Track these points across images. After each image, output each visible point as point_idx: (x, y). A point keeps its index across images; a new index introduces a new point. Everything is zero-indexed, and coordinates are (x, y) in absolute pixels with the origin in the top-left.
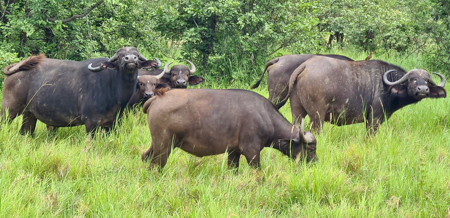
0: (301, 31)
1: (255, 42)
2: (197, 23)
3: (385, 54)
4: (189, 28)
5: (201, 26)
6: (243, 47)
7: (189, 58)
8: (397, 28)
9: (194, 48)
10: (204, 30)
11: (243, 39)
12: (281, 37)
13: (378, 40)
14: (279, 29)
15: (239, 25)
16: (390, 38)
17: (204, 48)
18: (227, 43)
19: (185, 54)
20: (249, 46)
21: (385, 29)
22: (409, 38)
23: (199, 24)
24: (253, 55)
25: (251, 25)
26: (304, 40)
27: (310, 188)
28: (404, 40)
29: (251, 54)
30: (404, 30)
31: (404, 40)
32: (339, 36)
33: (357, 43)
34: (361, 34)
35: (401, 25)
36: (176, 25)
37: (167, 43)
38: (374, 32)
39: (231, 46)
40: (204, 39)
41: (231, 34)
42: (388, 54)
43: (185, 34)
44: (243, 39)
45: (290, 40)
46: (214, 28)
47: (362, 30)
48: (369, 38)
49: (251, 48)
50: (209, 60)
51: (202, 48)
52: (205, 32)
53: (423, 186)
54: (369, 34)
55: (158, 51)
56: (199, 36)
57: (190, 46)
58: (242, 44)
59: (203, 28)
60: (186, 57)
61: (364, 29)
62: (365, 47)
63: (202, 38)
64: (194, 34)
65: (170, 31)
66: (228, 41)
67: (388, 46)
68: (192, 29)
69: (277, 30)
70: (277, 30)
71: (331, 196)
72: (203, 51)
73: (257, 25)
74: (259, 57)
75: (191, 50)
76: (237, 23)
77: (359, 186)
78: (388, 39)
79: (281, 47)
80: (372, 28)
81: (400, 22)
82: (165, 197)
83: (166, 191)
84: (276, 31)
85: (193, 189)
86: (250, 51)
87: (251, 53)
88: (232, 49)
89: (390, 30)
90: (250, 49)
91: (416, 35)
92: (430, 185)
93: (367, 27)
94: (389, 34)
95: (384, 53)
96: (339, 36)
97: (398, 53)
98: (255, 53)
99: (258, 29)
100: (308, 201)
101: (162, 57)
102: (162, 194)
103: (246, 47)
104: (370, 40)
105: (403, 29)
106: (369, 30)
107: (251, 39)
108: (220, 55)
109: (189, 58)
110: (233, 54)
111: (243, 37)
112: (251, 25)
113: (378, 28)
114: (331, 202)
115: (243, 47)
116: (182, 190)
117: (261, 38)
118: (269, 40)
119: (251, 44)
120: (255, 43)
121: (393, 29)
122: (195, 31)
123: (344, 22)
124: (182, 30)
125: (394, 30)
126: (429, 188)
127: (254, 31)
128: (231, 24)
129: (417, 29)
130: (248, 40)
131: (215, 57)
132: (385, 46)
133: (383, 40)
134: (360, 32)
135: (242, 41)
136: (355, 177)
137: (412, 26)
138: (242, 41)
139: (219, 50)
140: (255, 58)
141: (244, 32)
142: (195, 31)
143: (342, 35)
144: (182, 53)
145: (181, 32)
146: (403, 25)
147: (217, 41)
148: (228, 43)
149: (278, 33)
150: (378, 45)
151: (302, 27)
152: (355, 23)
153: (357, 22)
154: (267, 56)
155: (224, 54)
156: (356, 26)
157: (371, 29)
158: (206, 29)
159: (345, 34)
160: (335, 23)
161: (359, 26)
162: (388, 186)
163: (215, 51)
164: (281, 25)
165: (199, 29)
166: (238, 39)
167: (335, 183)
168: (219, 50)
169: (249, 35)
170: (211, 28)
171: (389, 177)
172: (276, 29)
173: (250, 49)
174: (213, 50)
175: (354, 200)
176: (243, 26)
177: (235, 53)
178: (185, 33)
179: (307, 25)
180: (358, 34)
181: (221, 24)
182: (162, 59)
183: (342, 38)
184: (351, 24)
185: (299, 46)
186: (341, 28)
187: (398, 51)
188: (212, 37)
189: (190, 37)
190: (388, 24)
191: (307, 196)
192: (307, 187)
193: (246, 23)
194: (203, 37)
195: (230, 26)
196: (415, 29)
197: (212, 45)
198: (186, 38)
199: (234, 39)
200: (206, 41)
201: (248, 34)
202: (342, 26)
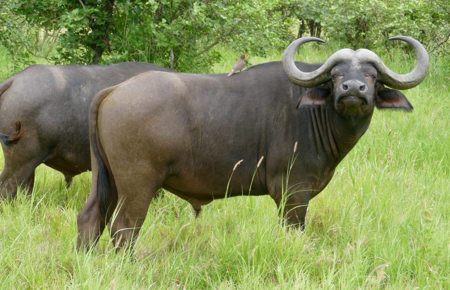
0: (249, 17)
1: (177, 33)
2: (84, 2)
3: (385, 56)
4: (70, 9)
5: (89, 6)
6: (156, 40)
7: (70, 57)
8: (405, 15)
9: (77, 40)
10: (95, 13)
11: (157, 29)
12: (217, 26)
13: (375, 33)
14: (213, 12)
15: (150, 5)
16: (394, 31)
17: (94, 42)
18: (130, 33)
19: (64, 50)
20: (166, 40)
21: (387, 18)
22: (423, 32)
23: (87, 3)
24: (172, 55)
25: (170, 6)
26: (253, 30)
27: (249, 257)
28: (416, 34)
29: (169, 53)
30: (413, 18)
31: (416, 34)
32: (314, 27)
33: (342, 39)
34: (349, 24)
35: (411, 11)
36: (49, 5)
37: (37, 34)
38: (369, 20)
39: (138, 39)
40: (94, 27)
41: (137, 19)
42: (391, 56)
43: (64, 19)
44: (157, 29)
45: (232, 31)
46: (110, 10)
47: (349, 18)
48: (361, 31)
49: (169, 42)
50: (103, 61)
51: (91, 41)
52: (95, 16)
53: (425, 254)
54: (361, 25)
55: (22, 48)
56: (86, 22)
57: (74, 39)
58: (155, 37)
59: (92, 9)
60: (66, 56)
61: (353, 17)
62: (354, 44)
63: (91, 26)
64: (78, 19)
65: (40, 15)
66: (133, 31)
67: (390, 43)
68: (76, 11)
69: (211, 14)
70: (211, 14)
71: (279, 269)
72: (93, 46)
73: (180, 7)
74: (182, 59)
75: (74, 44)
76: (147, 3)
77: (325, 254)
78: (390, 32)
79: (217, 43)
80: (365, 15)
81: (410, 6)
82: (21, 270)
83: (23, 261)
84: (210, 16)
85: (66, 259)
86: (167, 48)
87: (169, 50)
88: (139, 44)
89: (394, 19)
90: (167, 44)
91: (434, 26)
92: (436, 252)
93: (358, 13)
94: (391, 25)
95: (384, 54)
96: (314, 27)
97: (406, 56)
98: (177, 51)
99: (182, 13)
100: (245, 277)
101: (27, 56)
102: (15, 266)
103: (161, 41)
104: (363, 34)
105: (413, 16)
106: (360, 19)
107: (170, 28)
108: (120, 52)
109: (70, 57)
110: (141, 52)
111: (157, 25)
112: (170, 6)
113: (375, 15)
114: (281, 277)
115: (156, 40)
116: (47, 259)
117: (186, 27)
118: (199, 30)
119: (170, 37)
120: (175, 35)
121: (399, 17)
122: (80, 14)
123: (323, 5)
124: (59, 13)
125: (400, 18)
126: (435, 257)
127: (174, 17)
128: (136, 5)
129: (435, 16)
130: (165, 30)
131: (111, 57)
132: (386, 44)
133: (384, 33)
134: (346, 21)
135: (154, 32)
136: (321, 242)
137: (426, 12)
138: (154, 32)
139: (118, 46)
140: (176, 58)
141: (159, 16)
142: (80, 14)
143: (318, 25)
144: (59, 50)
145: (58, 16)
146: (415, 11)
147: (115, 32)
148: (132, 34)
149: (214, 19)
150: (376, 42)
151: (250, 11)
152: (340, 6)
153: (342, 5)
154: (195, 56)
155: (127, 52)
156: (340, 11)
157: (364, 17)
158: (96, 10)
159: (322, 24)
160: (308, 6)
161: (346, 12)
162: (371, 255)
163: (112, 47)
164: (217, 8)
165: (87, 10)
166: (148, 28)
167: (289, 249)
168: (118, 46)
169: (167, 23)
170: (106, 10)
171: (374, 240)
172: (209, 14)
173: (167, 44)
174: (108, 45)
175: (316, 274)
176: (156, 7)
177: (143, 49)
178: (63, 17)
179: (258, 10)
180: (342, 24)
181: (122, 4)
182: (26, 59)
183: (319, 30)
184: (333, 8)
185: (245, 40)
186: (317, 15)
187: (407, 53)
188: (107, 24)
189: (71, 24)
190: (390, 9)
191: (245, 269)
192: (246, 257)
193: (160, 3)
194: (93, 24)
195: (136, 7)
196: (433, 17)
197: (107, 38)
198: (65, 24)
199: (142, 28)
200: (97, 30)
201: (164, 21)
202: (319, 11)
